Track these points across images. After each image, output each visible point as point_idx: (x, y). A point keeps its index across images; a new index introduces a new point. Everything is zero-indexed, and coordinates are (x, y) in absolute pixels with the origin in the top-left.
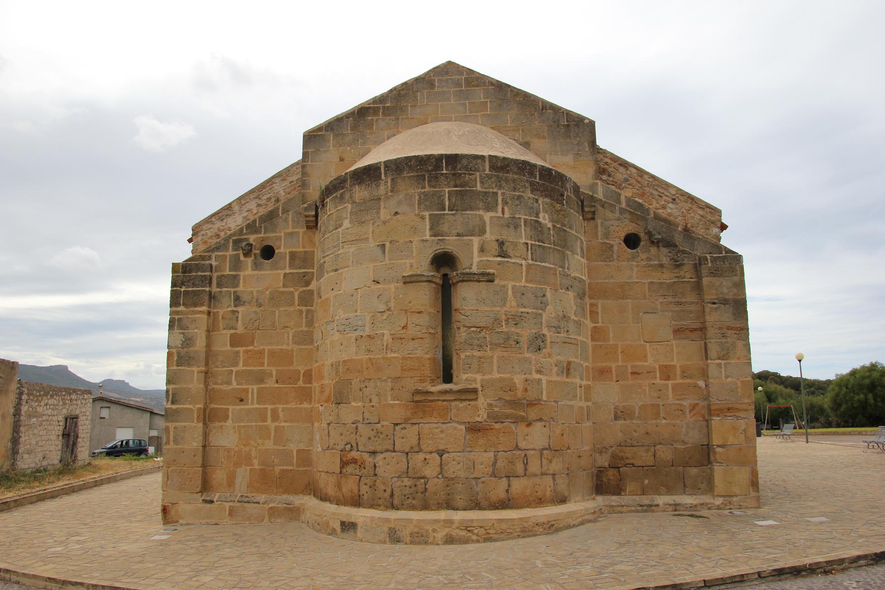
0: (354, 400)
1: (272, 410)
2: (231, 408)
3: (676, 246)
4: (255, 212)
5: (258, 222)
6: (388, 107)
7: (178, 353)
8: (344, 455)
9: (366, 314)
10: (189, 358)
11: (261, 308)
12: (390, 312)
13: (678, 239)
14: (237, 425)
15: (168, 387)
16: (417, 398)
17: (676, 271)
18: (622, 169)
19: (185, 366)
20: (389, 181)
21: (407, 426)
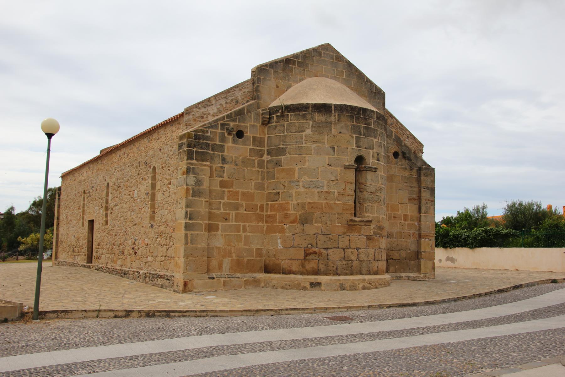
0: (316, 223)
1: (243, 226)
2: (220, 224)
3: (411, 160)
4: (224, 106)
5: (233, 114)
6: (300, 62)
7: (193, 189)
8: (307, 250)
9: (324, 180)
10: (200, 192)
11: (237, 167)
12: (337, 181)
13: (412, 157)
14: (224, 234)
15: (187, 209)
16: (350, 223)
17: (411, 172)
18: (390, 118)
19: (197, 197)
20: (337, 115)
21: (345, 236)
